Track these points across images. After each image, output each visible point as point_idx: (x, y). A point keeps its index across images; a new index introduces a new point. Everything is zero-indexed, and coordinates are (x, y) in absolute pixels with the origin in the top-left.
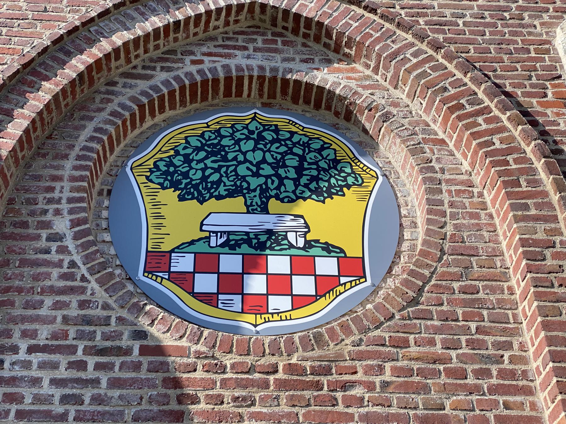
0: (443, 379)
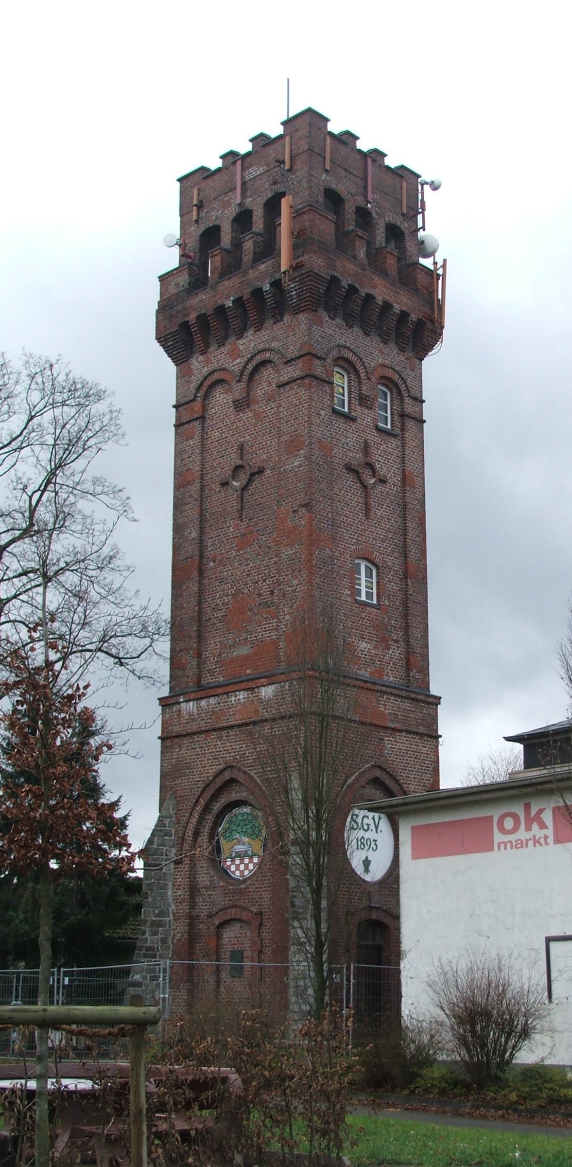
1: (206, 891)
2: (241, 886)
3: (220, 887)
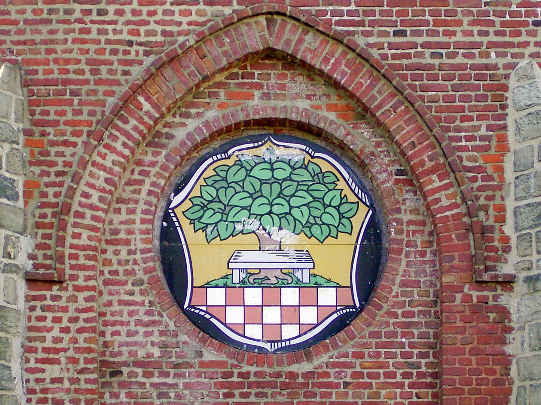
0: (399, 359)
1: (146, 375)
2: (295, 368)
3: (202, 364)
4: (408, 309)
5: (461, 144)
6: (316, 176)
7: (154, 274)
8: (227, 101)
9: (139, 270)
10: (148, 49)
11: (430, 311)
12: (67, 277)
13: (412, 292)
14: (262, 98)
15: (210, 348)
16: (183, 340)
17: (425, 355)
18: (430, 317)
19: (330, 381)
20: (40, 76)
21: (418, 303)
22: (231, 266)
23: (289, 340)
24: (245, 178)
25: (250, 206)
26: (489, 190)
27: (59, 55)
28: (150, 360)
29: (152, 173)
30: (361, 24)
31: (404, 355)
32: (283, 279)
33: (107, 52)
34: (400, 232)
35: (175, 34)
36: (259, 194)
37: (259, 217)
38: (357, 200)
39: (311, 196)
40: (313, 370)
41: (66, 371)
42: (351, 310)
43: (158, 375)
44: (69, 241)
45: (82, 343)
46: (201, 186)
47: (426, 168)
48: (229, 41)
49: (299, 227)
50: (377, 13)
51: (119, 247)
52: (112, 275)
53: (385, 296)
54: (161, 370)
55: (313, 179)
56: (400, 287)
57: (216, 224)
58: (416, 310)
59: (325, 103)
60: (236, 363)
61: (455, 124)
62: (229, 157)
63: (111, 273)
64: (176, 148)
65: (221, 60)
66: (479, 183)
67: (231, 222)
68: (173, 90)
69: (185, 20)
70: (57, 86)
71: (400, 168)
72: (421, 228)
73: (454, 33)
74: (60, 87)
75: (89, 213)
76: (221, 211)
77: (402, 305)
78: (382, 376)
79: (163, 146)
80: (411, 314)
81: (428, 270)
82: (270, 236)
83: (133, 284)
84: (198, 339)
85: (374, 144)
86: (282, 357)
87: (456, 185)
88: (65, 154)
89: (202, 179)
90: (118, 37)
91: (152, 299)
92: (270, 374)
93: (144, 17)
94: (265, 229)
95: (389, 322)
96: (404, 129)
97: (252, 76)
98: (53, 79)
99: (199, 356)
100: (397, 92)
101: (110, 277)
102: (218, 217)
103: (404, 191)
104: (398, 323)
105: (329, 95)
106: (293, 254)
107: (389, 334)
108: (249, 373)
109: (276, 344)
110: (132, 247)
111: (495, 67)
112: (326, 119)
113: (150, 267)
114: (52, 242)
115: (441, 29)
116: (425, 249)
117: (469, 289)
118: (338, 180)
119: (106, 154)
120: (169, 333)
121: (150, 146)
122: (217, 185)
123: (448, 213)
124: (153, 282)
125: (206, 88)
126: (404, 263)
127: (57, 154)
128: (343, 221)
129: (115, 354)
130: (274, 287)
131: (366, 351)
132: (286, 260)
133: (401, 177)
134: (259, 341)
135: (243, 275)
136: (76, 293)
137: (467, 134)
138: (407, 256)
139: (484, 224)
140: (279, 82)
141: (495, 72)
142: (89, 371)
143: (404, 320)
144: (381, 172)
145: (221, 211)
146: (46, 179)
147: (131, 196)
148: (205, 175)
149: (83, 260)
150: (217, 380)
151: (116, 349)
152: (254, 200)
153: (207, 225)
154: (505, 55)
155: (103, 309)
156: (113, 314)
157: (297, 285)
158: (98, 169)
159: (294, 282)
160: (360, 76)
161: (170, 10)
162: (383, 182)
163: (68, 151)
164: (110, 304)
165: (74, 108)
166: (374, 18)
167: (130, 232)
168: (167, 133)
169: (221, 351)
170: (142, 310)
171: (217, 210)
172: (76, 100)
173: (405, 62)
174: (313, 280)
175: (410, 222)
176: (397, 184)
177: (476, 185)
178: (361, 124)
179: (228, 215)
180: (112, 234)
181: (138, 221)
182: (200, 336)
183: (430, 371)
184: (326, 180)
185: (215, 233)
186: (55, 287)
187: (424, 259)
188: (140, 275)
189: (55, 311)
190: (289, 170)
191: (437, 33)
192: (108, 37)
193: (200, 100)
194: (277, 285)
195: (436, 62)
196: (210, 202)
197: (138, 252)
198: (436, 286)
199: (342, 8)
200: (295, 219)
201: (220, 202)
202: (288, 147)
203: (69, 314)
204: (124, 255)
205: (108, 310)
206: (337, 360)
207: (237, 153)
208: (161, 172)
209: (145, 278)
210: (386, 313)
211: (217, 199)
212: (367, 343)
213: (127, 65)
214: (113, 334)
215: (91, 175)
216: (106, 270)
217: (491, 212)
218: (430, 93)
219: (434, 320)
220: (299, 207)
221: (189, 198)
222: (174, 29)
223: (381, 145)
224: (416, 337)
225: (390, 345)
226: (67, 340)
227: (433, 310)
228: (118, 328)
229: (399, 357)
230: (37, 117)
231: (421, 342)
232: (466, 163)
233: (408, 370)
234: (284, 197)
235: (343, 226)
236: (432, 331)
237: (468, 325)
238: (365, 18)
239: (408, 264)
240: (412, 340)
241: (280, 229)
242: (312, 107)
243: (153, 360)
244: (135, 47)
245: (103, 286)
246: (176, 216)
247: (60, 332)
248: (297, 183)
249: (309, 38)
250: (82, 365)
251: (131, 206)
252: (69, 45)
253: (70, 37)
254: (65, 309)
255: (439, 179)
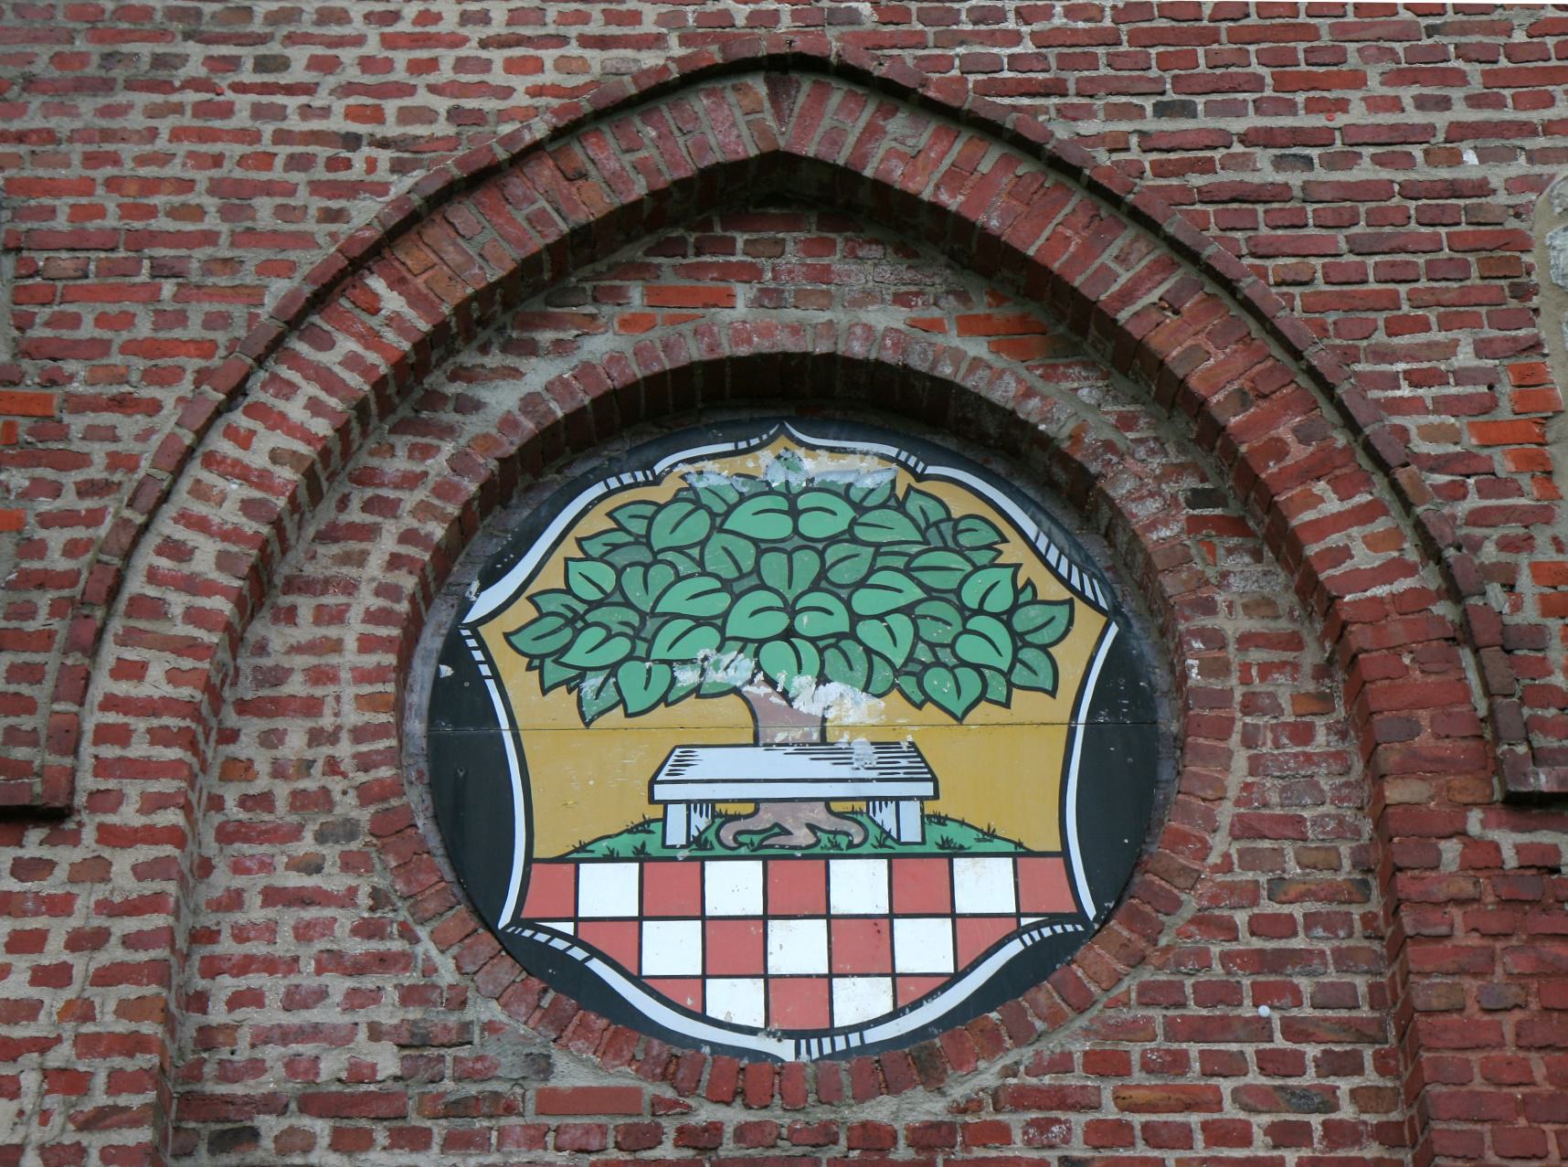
0: (1254, 1078)
3: (551, 1102)
4: (1268, 907)
5: (1398, 393)
6: (933, 530)
7: (395, 802)
8: (649, 310)
9: (345, 793)
10: (406, 155)
11: (1349, 914)
12: (80, 799)
13: (1279, 852)
14: (757, 303)
15: (580, 1044)
16: (485, 1017)
17: (1346, 1065)
18: (1350, 935)
19: (1010, 1154)
20: (61, 223)
21: (1302, 888)
22: (661, 792)
23: (861, 1028)
24: (708, 538)
25: (725, 615)
26: (1508, 521)
27: (128, 168)
28: (363, 1088)
29: (407, 506)
30: (1057, 89)
31: (1269, 1062)
32: (835, 833)
33: (279, 162)
34: (1220, 669)
35: (491, 119)
36: (754, 581)
37: (752, 647)
38: (1067, 595)
39: (920, 584)
40: (948, 1118)
41: (35, 1120)
42: (1069, 928)
43: (387, 1142)
44: (103, 684)
45: (109, 1018)
46: (567, 560)
47: (1289, 461)
48: (654, 134)
49: (883, 674)
50: (1103, 61)
51: (280, 723)
52: (248, 810)
53: (1184, 868)
54: (400, 1123)
55: (923, 536)
56: (1236, 838)
57: (613, 669)
58: (1297, 911)
59: (954, 315)
60: (669, 1093)
61: (1373, 340)
62: (657, 480)
63: (249, 803)
64: (486, 436)
65: (629, 182)
66: (1473, 502)
67: (662, 662)
68: (479, 260)
69: (520, 83)
70: (112, 250)
71: (1200, 486)
72: (1288, 656)
73: (1342, 106)
74: (122, 254)
75: (178, 602)
76: (630, 632)
77: (1250, 895)
78: (1199, 1138)
79: (448, 431)
80: (1286, 927)
81: (1325, 784)
82: (790, 701)
83: (321, 837)
84: (538, 1014)
85: (1112, 419)
86: (836, 1072)
87: (1395, 508)
88: (119, 432)
89: (570, 540)
90: (315, 125)
91: (381, 882)
92: (792, 1131)
93: (400, 75)
94: (771, 682)
95: (1207, 951)
96: (1208, 355)
97: (729, 247)
98: (101, 230)
99: (538, 1072)
100: (1177, 258)
101: (243, 816)
102: (620, 647)
103: (1221, 552)
104: (1239, 954)
105: (965, 292)
106: (862, 748)
107: (1208, 994)
108: (715, 1129)
109: (814, 1042)
110: (327, 721)
111: (1482, 188)
112: (957, 356)
113: (380, 781)
114: (40, 692)
115: (1300, 98)
116: (1307, 719)
117: (1484, 824)
118: (1005, 540)
119: (252, 433)
120: (435, 996)
121: (404, 432)
122: (619, 558)
123: (1380, 591)
124: (391, 829)
125: (586, 279)
126: (1240, 760)
127: (91, 434)
128: (1027, 654)
129: (236, 1070)
130: (804, 857)
131: (1135, 1050)
132: (844, 771)
133: (1207, 512)
134: (752, 1031)
135: (700, 822)
136: (107, 853)
137: (1415, 366)
138: (1249, 740)
139: (1508, 620)
140: (809, 261)
141: (1483, 200)
142: (125, 1117)
143: (1257, 943)
144: (1142, 498)
145: (630, 632)
146: (45, 505)
147: (334, 571)
148: (582, 530)
149: (145, 746)
150: (602, 1157)
151: (243, 1053)
152: (736, 598)
153: (583, 672)
154: (1508, 155)
155: (209, 920)
156: (240, 935)
157: (880, 851)
158: (222, 475)
159: (872, 840)
160: (1059, 218)
161: (478, 58)
162: (1153, 525)
163: (128, 425)
164: (234, 900)
165: (159, 307)
166: (1094, 74)
167: (321, 676)
168: (458, 396)
169: (618, 1055)
170: (345, 920)
171: (616, 628)
172: (168, 288)
173: (1196, 180)
174: (935, 833)
175: (1246, 641)
176: (1198, 532)
177: (1462, 508)
178: (1069, 366)
179: (651, 642)
180: (260, 684)
181: (351, 643)
182: (545, 1003)
183: (1372, 1119)
184: (964, 540)
185: (610, 695)
186: (34, 836)
187: (1308, 749)
188: (347, 806)
189: (24, 913)
190: (846, 513)
191: (1291, 108)
192: (285, 125)
193: (566, 310)
194: (817, 850)
195: (1295, 179)
196: (593, 605)
197: (344, 736)
198: (1357, 832)
199: (995, 50)
200: (869, 652)
201: (628, 604)
202: (844, 451)
203: (75, 922)
204: (295, 742)
205: (227, 921)
206: (1033, 1081)
207: (683, 468)
208: (436, 502)
209: (364, 816)
210: (1193, 921)
211: (617, 598)
212: (1135, 1020)
213: (340, 196)
214: (235, 1002)
215: (199, 491)
216: (231, 794)
217: (1525, 582)
218: (1281, 261)
219: (1366, 943)
220: (881, 617)
221: (530, 591)
222: (489, 105)
223: (1136, 423)
224: (1307, 1001)
225: (1223, 1028)
226: (54, 1010)
227: (1356, 911)
228: (254, 980)
229: (1253, 1067)
230: (39, 332)
231: (1326, 1019)
232: (1422, 447)
233: (1292, 1117)
234: (834, 589)
235: (1025, 672)
236: (1361, 983)
237: (1499, 945)
238: (1064, 74)
239: (1255, 766)
240: (1295, 1012)
241: (822, 679)
242: (913, 324)
243: (372, 1088)
244: (366, 150)
245: (215, 845)
246: (482, 647)
247: (34, 982)
248: (871, 550)
249: (898, 125)
250: (99, 1097)
251: (331, 600)
252: (162, 144)
253: (165, 125)
254: (60, 906)
255: (1335, 492)
